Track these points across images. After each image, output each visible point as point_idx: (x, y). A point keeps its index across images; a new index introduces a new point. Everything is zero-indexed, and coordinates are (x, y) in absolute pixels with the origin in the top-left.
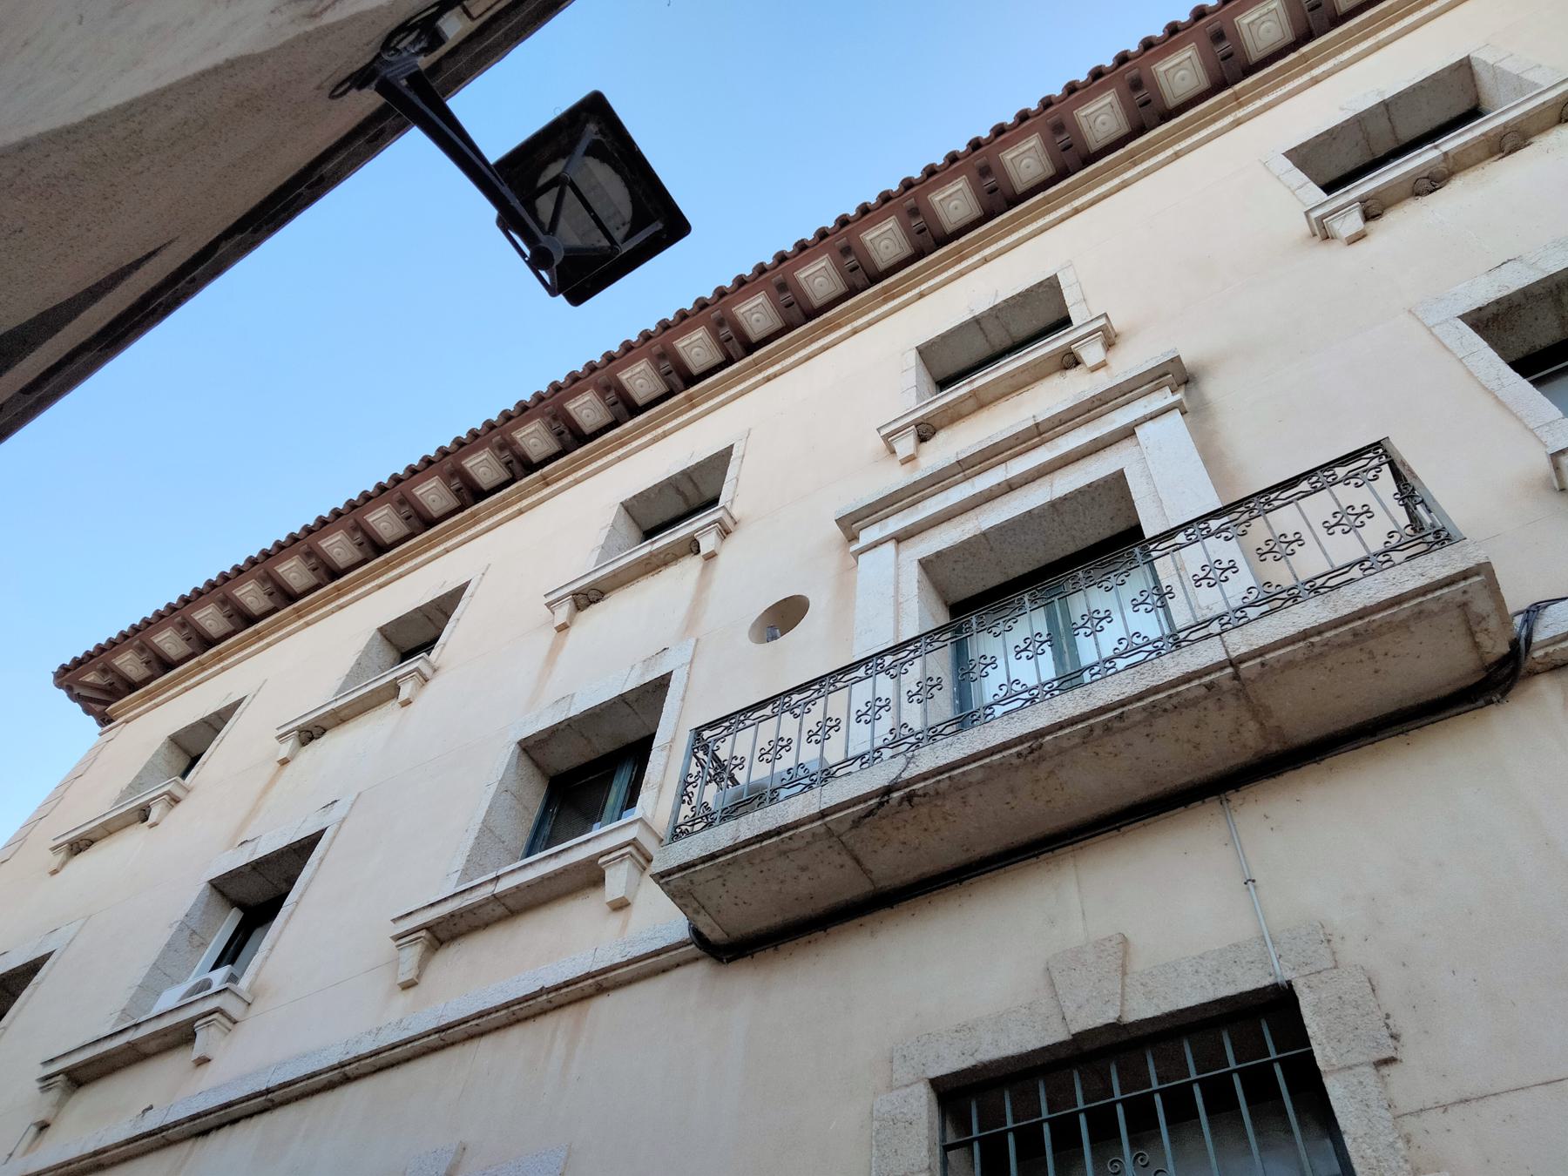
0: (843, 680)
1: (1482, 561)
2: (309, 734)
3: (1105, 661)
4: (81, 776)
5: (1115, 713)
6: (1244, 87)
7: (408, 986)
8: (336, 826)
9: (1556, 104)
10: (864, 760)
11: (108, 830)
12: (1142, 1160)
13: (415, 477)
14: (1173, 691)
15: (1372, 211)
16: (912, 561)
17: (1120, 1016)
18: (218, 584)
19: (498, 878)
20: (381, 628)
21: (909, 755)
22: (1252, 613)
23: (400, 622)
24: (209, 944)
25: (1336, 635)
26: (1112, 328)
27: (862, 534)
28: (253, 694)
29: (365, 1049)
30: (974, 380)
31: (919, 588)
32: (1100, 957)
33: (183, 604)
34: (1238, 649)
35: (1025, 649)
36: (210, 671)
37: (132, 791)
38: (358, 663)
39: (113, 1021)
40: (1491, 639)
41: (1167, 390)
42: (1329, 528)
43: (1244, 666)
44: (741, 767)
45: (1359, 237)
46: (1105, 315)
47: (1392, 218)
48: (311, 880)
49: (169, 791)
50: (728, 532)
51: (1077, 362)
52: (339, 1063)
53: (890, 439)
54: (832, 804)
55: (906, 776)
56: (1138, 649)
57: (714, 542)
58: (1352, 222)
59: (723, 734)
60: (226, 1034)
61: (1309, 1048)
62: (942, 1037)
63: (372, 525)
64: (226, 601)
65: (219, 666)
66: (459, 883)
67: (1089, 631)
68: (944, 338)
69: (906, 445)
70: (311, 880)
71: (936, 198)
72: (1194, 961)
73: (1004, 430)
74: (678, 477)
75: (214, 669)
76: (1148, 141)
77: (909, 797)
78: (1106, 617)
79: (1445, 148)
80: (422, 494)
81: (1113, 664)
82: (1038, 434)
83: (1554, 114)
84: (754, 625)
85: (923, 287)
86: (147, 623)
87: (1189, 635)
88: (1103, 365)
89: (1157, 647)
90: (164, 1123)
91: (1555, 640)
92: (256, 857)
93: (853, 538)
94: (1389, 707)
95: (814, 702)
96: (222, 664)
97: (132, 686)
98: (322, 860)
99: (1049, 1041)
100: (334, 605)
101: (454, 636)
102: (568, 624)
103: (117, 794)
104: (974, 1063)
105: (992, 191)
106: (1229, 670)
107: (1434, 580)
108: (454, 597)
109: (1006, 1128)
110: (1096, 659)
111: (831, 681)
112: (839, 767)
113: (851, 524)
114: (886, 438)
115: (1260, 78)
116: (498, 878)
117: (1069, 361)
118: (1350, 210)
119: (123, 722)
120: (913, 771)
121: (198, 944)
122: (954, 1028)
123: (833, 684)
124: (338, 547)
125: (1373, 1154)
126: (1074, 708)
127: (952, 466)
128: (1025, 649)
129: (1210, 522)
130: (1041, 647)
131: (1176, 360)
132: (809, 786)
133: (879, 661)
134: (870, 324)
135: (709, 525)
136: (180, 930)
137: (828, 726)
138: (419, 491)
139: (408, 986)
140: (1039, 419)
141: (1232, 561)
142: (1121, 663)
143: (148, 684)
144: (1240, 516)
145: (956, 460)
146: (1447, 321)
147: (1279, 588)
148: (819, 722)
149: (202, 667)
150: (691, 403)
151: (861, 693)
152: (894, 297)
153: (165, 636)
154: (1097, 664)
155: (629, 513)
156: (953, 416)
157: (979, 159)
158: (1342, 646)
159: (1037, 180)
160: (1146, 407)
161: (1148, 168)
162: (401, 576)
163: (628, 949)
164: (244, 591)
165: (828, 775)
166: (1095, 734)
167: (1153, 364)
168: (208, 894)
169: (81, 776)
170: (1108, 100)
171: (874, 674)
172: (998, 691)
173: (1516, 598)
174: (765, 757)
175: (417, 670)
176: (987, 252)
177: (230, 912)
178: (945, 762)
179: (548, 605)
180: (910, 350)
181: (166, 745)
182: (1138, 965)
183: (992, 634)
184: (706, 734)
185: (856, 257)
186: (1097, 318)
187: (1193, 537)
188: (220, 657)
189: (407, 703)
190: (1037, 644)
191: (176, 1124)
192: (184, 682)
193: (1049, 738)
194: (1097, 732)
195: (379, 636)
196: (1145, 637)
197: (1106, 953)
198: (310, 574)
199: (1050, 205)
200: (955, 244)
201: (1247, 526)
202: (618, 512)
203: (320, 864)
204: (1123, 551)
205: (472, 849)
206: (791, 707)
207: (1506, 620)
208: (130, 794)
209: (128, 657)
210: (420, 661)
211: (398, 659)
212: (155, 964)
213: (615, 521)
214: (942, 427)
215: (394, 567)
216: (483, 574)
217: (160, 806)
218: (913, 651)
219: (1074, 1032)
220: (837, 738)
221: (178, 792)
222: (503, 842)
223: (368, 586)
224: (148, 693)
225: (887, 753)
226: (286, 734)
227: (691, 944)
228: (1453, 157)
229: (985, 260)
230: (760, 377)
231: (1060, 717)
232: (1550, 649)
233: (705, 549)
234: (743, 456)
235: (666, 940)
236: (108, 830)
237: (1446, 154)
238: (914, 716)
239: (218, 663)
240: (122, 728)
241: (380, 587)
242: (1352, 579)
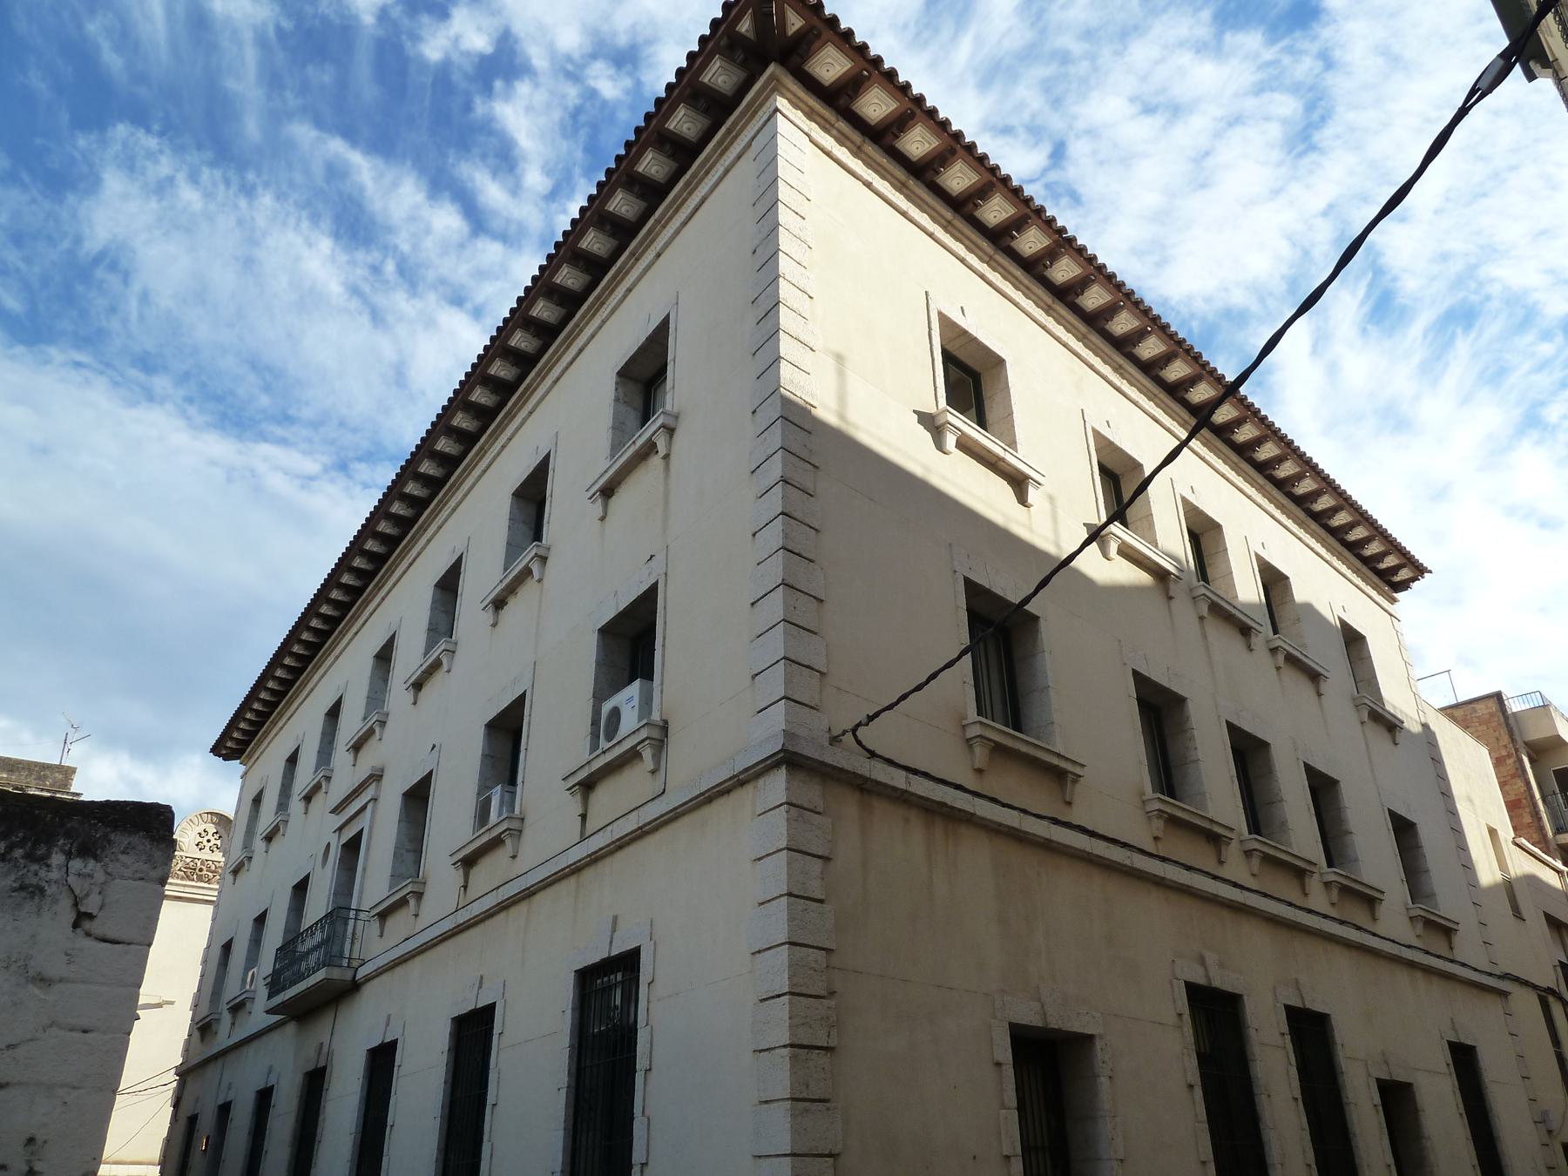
6: (535, 366)
16: (1202, 961)
50: (546, 558)
63: (709, 84)
108: (661, 335)
124: (686, 122)
153: (518, 338)
164: (645, 164)
198: (611, 240)
236: (512, 589)
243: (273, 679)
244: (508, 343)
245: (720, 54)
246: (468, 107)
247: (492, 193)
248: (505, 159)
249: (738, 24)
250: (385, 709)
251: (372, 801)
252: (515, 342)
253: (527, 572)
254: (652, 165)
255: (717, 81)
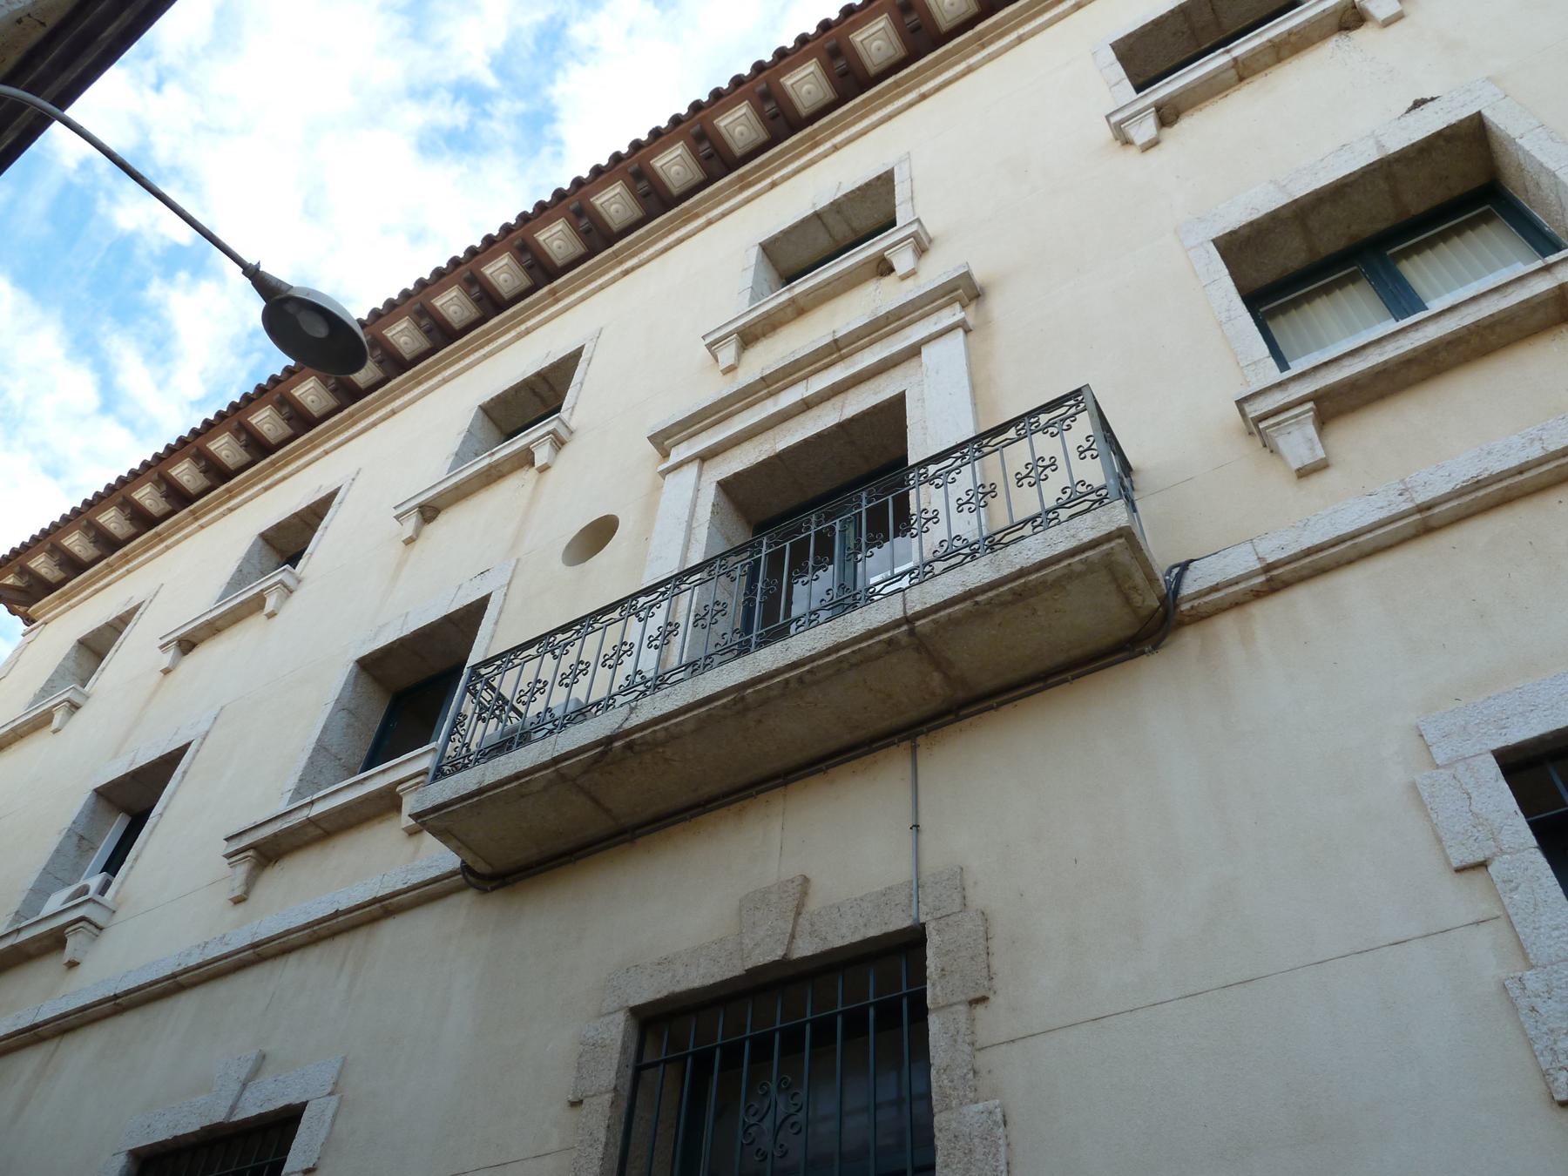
0: (688, 582)
1: (1122, 525)
2: (187, 645)
3: (1048, 512)
4: (4, 677)
5: (807, 668)
7: (238, 901)
8: (200, 740)
9: (1335, 12)
10: (799, 623)
11: (212, 629)
12: (785, 1084)
13: (293, 378)
14: (856, 648)
15: (1167, 115)
17: (785, 954)
18: (241, 406)
19: (312, 803)
20: (263, 533)
21: (633, 704)
22: (939, 566)
23: (279, 527)
24: (98, 848)
25: (997, 595)
26: (926, 234)
27: (673, 452)
28: (149, 600)
29: (192, 962)
30: (793, 287)
31: (713, 512)
32: (781, 898)
33: (87, 508)
34: (914, 607)
35: (1027, 476)
36: (118, 573)
37: (45, 694)
38: (240, 570)
39: (8, 923)
40: (1140, 595)
41: (957, 306)
42: (1081, 453)
43: (918, 623)
44: (629, 653)
45: (1154, 143)
46: (918, 220)
47: (1186, 124)
48: (174, 793)
49: (281, 580)
50: (563, 443)
51: (891, 270)
52: (172, 974)
53: (713, 348)
54: (563, 752)
55: (627, 726)
56: (956, 552)
57: (546, 455)
58: (1146, 129)
59: (573, 638)
60: (94, 940)
61: (1530, 819)
62: (646, 969)
63: (440, 309)
64: (24, 571)
65: (125, 569)
66: (291, 800)
67: (973, 507)
68: (787, 234)
69: (728, 354)
70: (174, 793)
71: (858, 38)
72: (855, 902)
73: (806, 346)
74: (533, 379)
75: (121, 571)
76: (995, 23)
77: (629, 746)
78: (1022, 478)
79: (1236, 53)
80: (443, 304)
81: (1056, 514)
82: (836, 350)
83: (1334, 21)
84: (569, 546)
85: (776, 176)
86: (55, 527)
87: (883, 588)
88: (912, 273)
89: (1101, 495)
90: (35, 1022)
91: (1200, 594)
92: (133, 768)
93: (666, 455)
94: (1060, 658)
95: (572, 643)
96: (127, 567)
97: (49, 587)
98: (185, 772)
99: (728, 975)
100: (225, 507)
101: (322, 547)
102: (415, 537)
103: (30, 697)
104: (666, 994)
105: (915, 30)
106: (905, 628)
107: (1082, 542)
109: (868, 1002)
110: (1038, 510)
111: (678, 583)
112: (1006, 532)
113: (663, 440)
114: (709, 346)
115: (568, 279)
116: (312, 803)
117: (883, 267)
118: (1145, 116)
119: (42, 624)
120: (635, 721)
121: (87, 848)
122: (657, 961)
123: (978, 450)
124: (742, 124)
125: (950, 1084)
126: (773, 662)
127: (756, 382)
128: (1027, 476)
129: (1040, 416)
130: (1044, 473)
131: (967, 276)
132: (551, 732)
133: (723, 562)
134: (724, 215)
135: (543, 436)
136: (68, 836)
137: (580, 668)
138: (297, 392)
139: (238, 901)
140: (838, 335)
141: (993, 484)
142: (1064, 514)
143: (65, 585)
144: (955, 462)
145: (761, 376)
146: (1202, 244)
147: (1090, 488)
148: (661, 627)
149: (111, 569)
150: (555, 297)
151: (1018, 455)
152: (750, 185)
154: (1039, 516)
155: (488, 415)
156: (798, 310)
157: (829, 42)
158: (1004, 604)
159: (820, 105)
160: (936, 324)
161: (994, 52)
162: (284, 479)
163: (409, 877)
165: (581, 713)
166: (792, 685)
167: (944, 279)
168: (94, 799)
169: (4, 677)
170: (882, 25)
171: (916, 485)
172: (1061, 495)
173: (1162, 556)
174: (654, 643)
175: (281, 582)
176: (925, 88)
177: (117, 816)
178: (660, 713)
179: (397, 517)
180: (754, 246)
181: (76, 648)
182: (813, 905)
183: (1048, 434)
184: (483, 671)
185: (711, 142)
186: (911, 223)
187: (1023, 432)
188: (126, 559)
189: (271, 615)
190: (980, 496)
191: (46, 1022)
192: (94, 584)
193: (750, 691)
194: (792, 685)
195: (261, 542)
196: (1089, 485)
197: (787, 894)
199: (901, 89)
200: (809, 130)
201: (1072, 421)
202: (476, 415)
203: (183, 777)
204: (897, 474)
205: (305, 768)
206: (727, 570)
207: (1150, 577)
208: (43, 697)
209: (42, 560)
210: (284, 574)
211: (503, 438)
212: (44, 869)
213: (471, 425)
214: (202, 641)
215: (279, 469)
216: (353, 480)
217: (61, 712)
218: (1073, 406)
219: (746, 968)
220: (998, 504)
221: (77, 699)
222: (340, 759)
223: (256, 489)
224: (64, 594)
225: (620, 700)
226: (167, 644)
227: (459, 874)
228: (1243, 63)
229: (836, 148)
230: (618, 270)
231: (760, 671)
232: (1196, 603)
233: (539, 462)
234: (591, 358)
235: (440, 869)
236: (212, 629)
237: (1235, 59)
238: (648, 662)
239: (124, 566)
240: (42, 630)
241: (266, 489)
242: (1023, 536)
243: (157, 484)
244: (133, 495)
245: (750, 101)
246: (141, 285)
247: (133, 371)
248: (160, 349)
249: (853, 33)
250: (87, 688)
251: (960, 332)
252: (216, 446)
253: (257, 603)
254: (613, 202)
255: (670, 170)
